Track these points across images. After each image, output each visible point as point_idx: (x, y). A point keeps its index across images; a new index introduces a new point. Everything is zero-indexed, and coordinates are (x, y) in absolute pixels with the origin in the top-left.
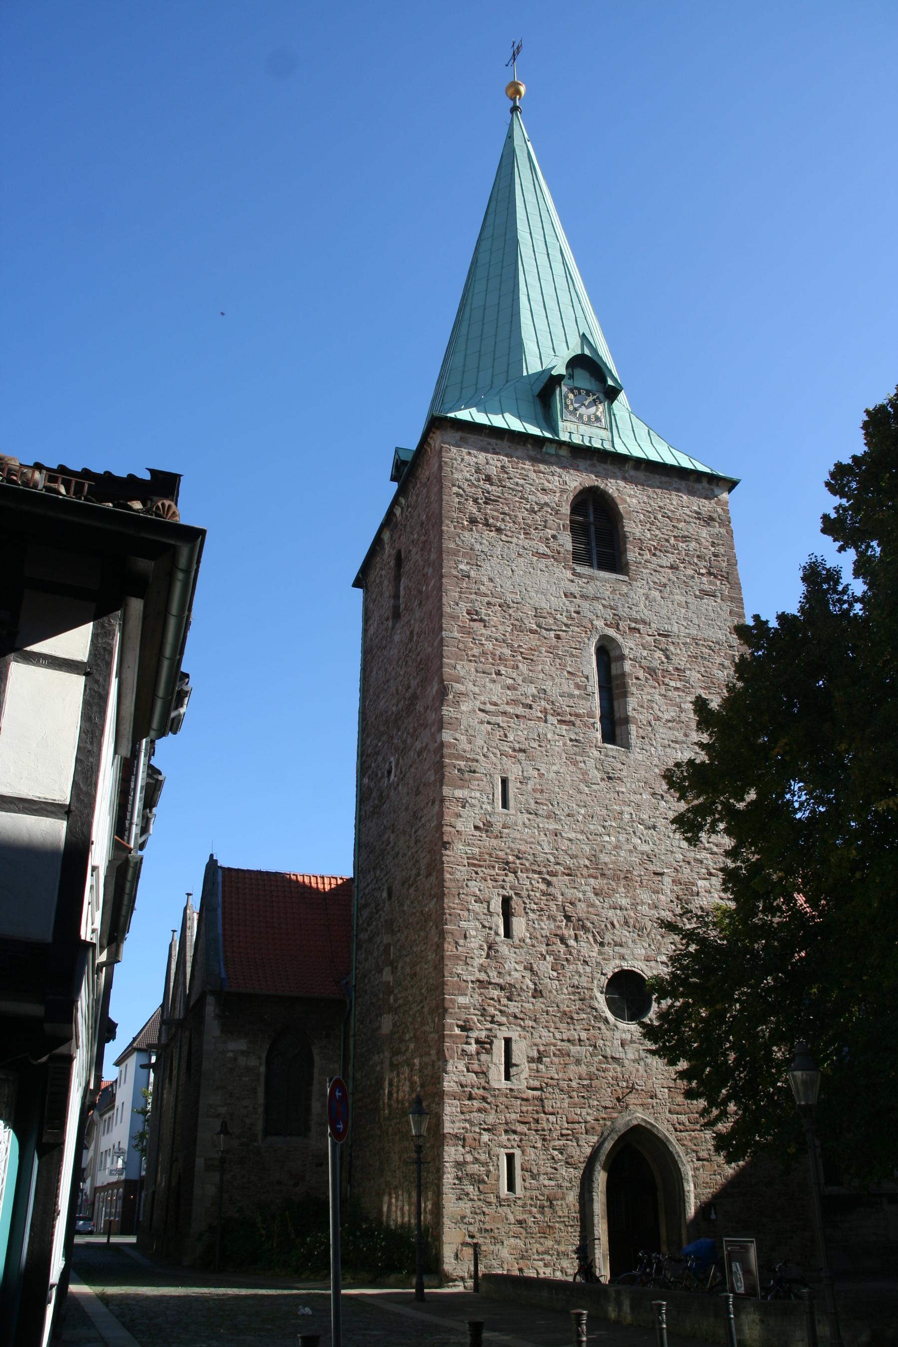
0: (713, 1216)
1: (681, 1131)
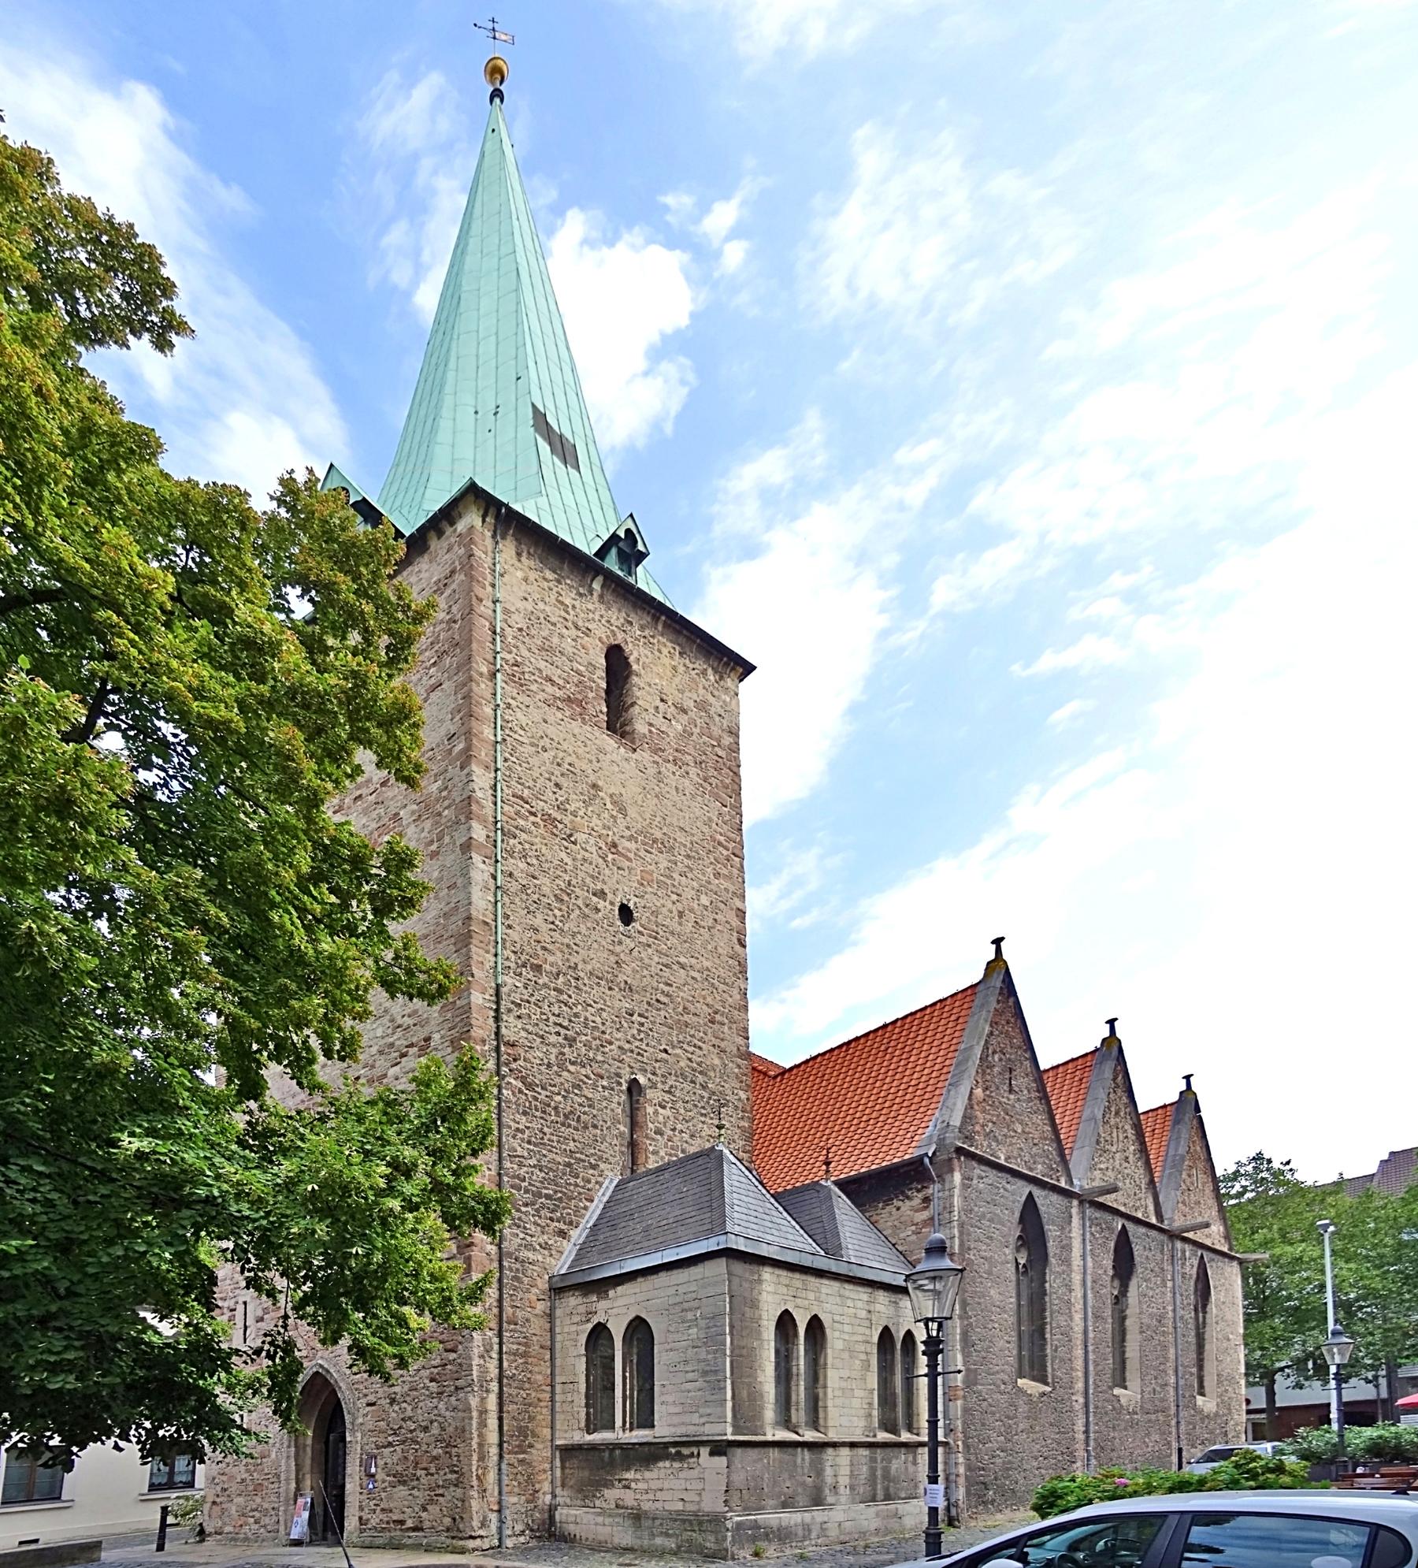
0: (373, 1470)
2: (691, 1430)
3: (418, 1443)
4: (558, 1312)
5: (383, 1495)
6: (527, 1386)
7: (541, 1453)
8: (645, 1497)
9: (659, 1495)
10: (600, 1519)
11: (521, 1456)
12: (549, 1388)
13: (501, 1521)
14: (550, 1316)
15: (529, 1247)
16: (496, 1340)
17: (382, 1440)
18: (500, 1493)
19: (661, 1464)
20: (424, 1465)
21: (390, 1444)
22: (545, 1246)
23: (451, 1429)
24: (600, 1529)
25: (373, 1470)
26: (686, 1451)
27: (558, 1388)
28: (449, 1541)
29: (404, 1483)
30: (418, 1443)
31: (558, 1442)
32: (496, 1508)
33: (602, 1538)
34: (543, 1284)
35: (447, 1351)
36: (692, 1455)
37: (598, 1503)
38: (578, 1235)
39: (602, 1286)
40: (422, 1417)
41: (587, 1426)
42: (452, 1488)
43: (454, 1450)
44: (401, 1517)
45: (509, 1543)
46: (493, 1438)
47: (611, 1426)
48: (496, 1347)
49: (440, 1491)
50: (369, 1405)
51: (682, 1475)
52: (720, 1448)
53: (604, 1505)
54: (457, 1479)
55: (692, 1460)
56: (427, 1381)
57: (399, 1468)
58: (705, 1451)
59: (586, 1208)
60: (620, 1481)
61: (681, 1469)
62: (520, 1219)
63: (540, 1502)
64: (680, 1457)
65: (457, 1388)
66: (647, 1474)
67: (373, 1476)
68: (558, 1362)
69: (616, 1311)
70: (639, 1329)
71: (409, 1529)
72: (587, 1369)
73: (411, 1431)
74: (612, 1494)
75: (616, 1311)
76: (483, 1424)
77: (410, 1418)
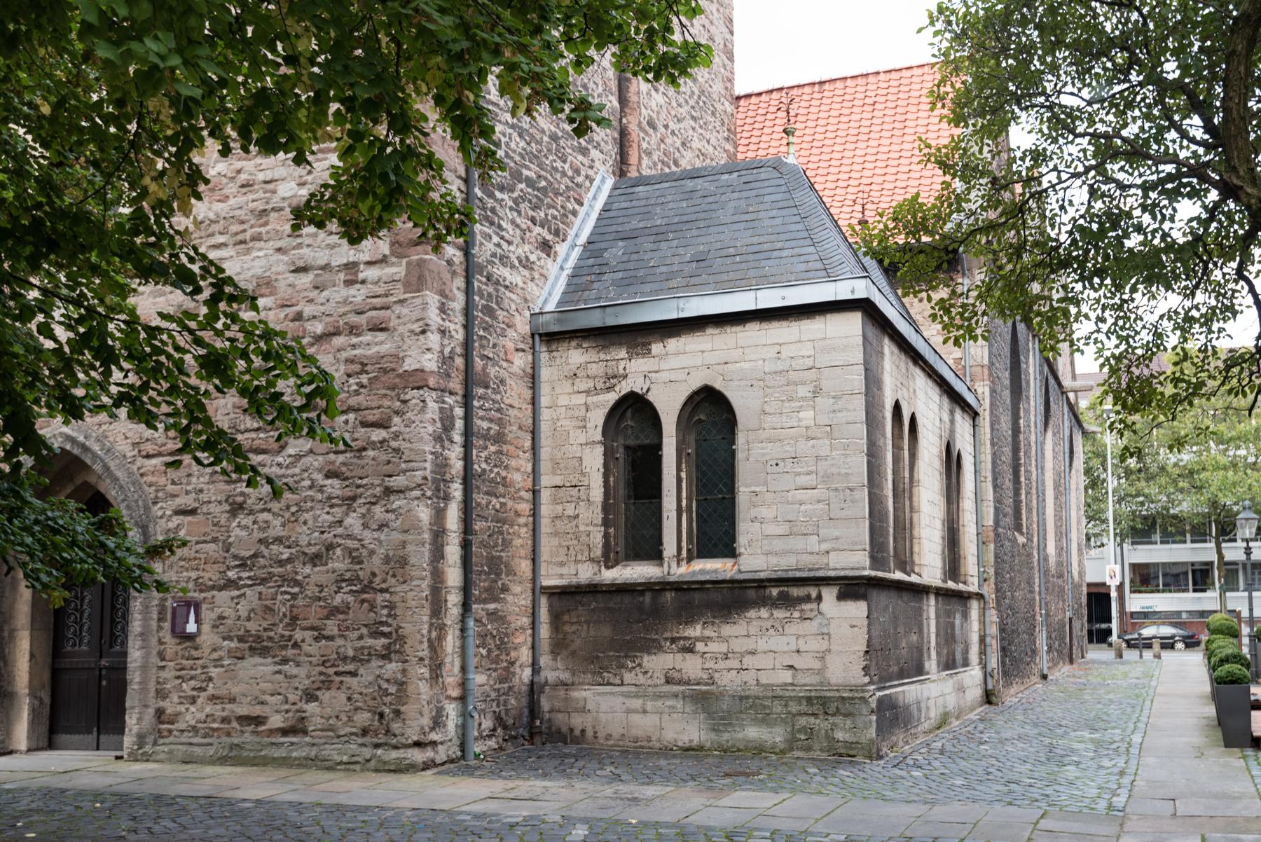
0: (191, 627)
1: (148, 456)
2: (807, 560)
3: (297, 583)
4: (545, 373)
5: (214, 672)
6: (501, 489)
7: (518, 599)
8: (722, 665)
9: (748, 661)
10: (637, 703)
11: (492, 606)
12: (528, 496)
13: (465, 715)
14: (533, 379)
15: (504, 260)
16: (459, 412)
17: (211, 574)
18: (464, 669)
19: (752, 613)
20: (312, 621)
21: (230, 584)
22: (526, 264)
23: (377, 561)
24: (637, 719)
25: (191, 627)
26: (795, 592)
27: (545, 496)
28: (367, 752)
29: (264, 652)
30: (297, 583)
31: (546, 583)
32: (455, 693)
33: (640, 733)
34: (522, 325)
35: (365, 424)
36: (807, 599)
37: (628, 677)
38: (568, 254)
39: (640, 335)
40: (305, 536)
41: (606, 555)
42: (375, 663)
43: (380, 598)
44: (257, 711)
45: (478, 748)
46: (453, 576)
47: (655, 555)
48: (459, 424)
49: (350, 667)
50: (180, 512)
51: (790, 629)
52: (852, 588)
53: (641, 679)
54: (387, 647)
55: (806, 607)
56: (318, 477)
57: (253, 626)
58: (829, 594)
59: (574, 213)
60: (673, 640)
61: (790, 621)
62: (493, 210)
63: (516, 681)
64: (787, 602)
65: (388, 491)
66: (727, 630)
67: (191, 637)
68: (545, 453)
69: (668, 375)
70: (711, 410)
71: (271, 732)
72: (606, 465)
73: (281, 563)
74: (658, 663)
75: (668, 375)
76: (438, 554)
77: (279, 540)
